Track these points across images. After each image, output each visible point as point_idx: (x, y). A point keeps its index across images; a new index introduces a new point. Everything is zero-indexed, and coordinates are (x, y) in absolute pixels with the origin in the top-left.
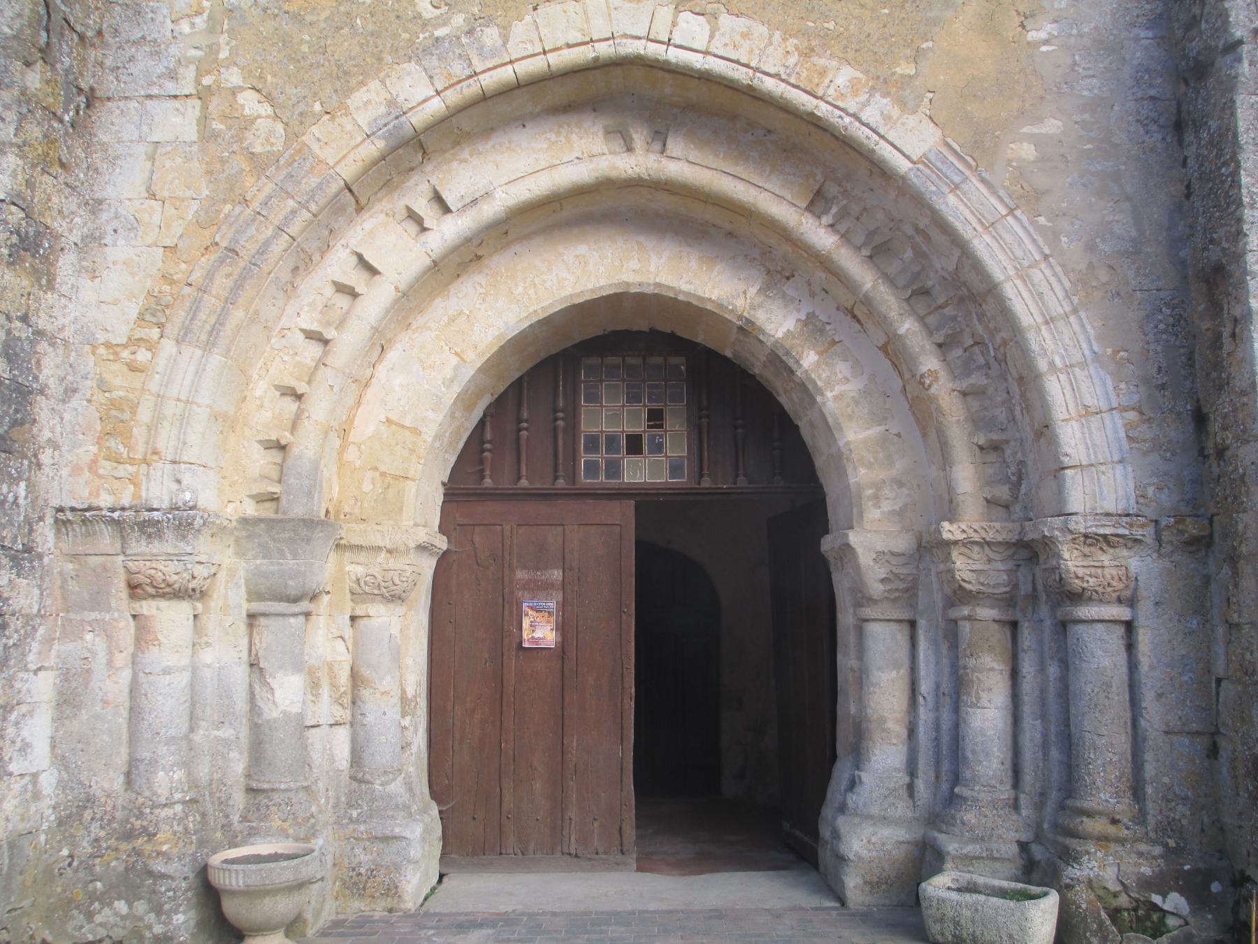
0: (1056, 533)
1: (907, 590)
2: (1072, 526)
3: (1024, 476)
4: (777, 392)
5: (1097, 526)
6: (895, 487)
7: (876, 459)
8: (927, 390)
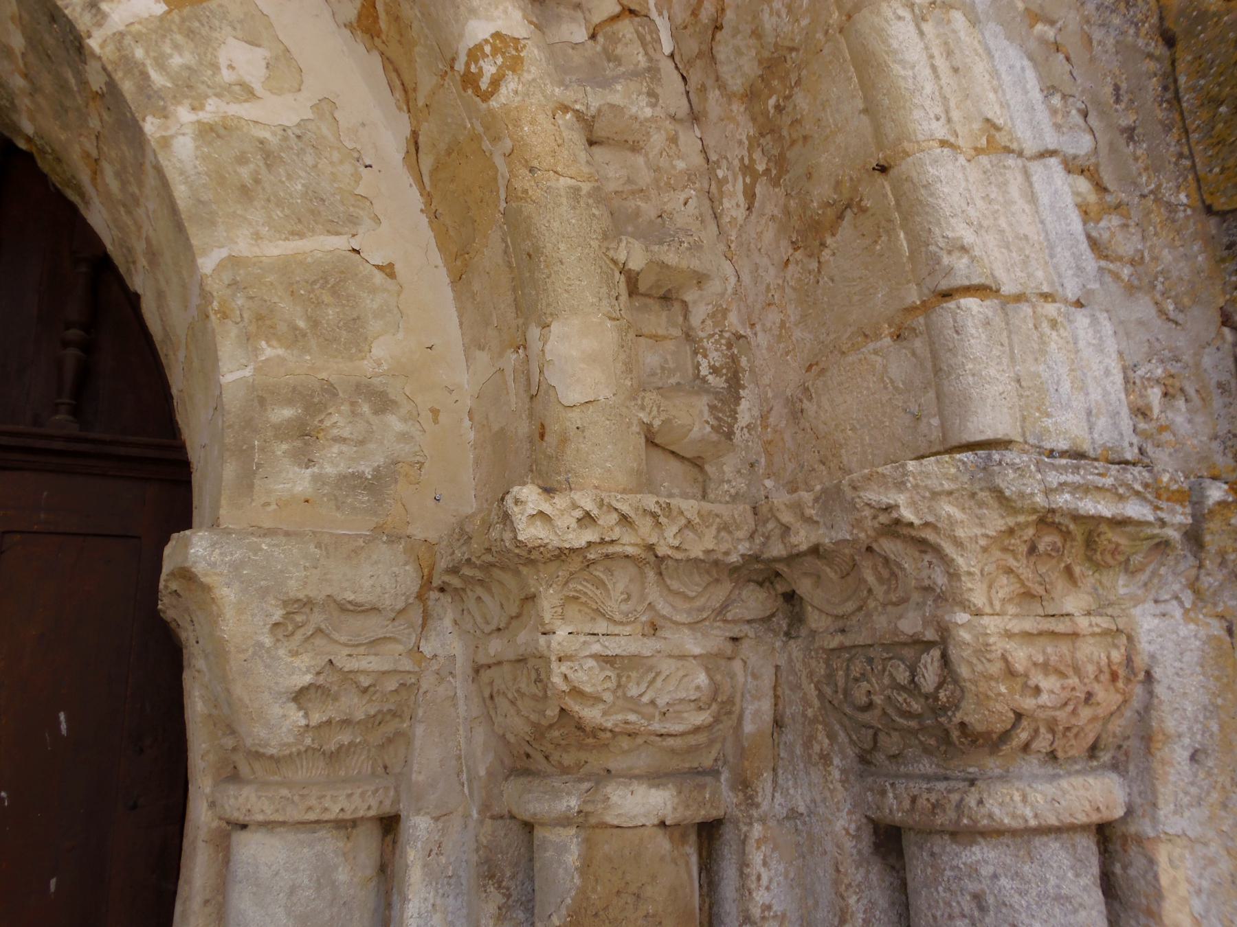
0: (948, 508)
1: (375, 721)
2: (1010, 483)
3: (745, 378)
4: (82, 195)
5: (1075, 488)
6: (366, 409)
7: (315, 323)
8: (486, 96)
